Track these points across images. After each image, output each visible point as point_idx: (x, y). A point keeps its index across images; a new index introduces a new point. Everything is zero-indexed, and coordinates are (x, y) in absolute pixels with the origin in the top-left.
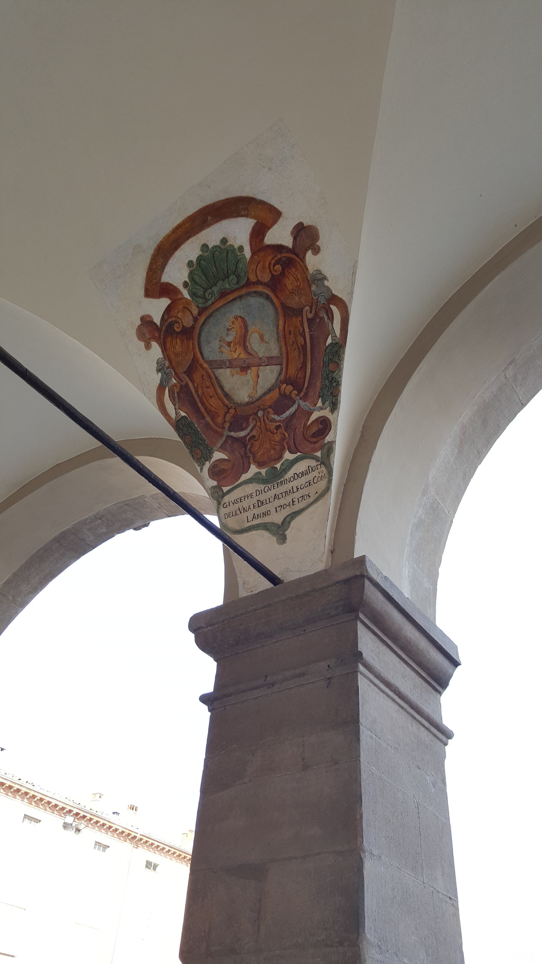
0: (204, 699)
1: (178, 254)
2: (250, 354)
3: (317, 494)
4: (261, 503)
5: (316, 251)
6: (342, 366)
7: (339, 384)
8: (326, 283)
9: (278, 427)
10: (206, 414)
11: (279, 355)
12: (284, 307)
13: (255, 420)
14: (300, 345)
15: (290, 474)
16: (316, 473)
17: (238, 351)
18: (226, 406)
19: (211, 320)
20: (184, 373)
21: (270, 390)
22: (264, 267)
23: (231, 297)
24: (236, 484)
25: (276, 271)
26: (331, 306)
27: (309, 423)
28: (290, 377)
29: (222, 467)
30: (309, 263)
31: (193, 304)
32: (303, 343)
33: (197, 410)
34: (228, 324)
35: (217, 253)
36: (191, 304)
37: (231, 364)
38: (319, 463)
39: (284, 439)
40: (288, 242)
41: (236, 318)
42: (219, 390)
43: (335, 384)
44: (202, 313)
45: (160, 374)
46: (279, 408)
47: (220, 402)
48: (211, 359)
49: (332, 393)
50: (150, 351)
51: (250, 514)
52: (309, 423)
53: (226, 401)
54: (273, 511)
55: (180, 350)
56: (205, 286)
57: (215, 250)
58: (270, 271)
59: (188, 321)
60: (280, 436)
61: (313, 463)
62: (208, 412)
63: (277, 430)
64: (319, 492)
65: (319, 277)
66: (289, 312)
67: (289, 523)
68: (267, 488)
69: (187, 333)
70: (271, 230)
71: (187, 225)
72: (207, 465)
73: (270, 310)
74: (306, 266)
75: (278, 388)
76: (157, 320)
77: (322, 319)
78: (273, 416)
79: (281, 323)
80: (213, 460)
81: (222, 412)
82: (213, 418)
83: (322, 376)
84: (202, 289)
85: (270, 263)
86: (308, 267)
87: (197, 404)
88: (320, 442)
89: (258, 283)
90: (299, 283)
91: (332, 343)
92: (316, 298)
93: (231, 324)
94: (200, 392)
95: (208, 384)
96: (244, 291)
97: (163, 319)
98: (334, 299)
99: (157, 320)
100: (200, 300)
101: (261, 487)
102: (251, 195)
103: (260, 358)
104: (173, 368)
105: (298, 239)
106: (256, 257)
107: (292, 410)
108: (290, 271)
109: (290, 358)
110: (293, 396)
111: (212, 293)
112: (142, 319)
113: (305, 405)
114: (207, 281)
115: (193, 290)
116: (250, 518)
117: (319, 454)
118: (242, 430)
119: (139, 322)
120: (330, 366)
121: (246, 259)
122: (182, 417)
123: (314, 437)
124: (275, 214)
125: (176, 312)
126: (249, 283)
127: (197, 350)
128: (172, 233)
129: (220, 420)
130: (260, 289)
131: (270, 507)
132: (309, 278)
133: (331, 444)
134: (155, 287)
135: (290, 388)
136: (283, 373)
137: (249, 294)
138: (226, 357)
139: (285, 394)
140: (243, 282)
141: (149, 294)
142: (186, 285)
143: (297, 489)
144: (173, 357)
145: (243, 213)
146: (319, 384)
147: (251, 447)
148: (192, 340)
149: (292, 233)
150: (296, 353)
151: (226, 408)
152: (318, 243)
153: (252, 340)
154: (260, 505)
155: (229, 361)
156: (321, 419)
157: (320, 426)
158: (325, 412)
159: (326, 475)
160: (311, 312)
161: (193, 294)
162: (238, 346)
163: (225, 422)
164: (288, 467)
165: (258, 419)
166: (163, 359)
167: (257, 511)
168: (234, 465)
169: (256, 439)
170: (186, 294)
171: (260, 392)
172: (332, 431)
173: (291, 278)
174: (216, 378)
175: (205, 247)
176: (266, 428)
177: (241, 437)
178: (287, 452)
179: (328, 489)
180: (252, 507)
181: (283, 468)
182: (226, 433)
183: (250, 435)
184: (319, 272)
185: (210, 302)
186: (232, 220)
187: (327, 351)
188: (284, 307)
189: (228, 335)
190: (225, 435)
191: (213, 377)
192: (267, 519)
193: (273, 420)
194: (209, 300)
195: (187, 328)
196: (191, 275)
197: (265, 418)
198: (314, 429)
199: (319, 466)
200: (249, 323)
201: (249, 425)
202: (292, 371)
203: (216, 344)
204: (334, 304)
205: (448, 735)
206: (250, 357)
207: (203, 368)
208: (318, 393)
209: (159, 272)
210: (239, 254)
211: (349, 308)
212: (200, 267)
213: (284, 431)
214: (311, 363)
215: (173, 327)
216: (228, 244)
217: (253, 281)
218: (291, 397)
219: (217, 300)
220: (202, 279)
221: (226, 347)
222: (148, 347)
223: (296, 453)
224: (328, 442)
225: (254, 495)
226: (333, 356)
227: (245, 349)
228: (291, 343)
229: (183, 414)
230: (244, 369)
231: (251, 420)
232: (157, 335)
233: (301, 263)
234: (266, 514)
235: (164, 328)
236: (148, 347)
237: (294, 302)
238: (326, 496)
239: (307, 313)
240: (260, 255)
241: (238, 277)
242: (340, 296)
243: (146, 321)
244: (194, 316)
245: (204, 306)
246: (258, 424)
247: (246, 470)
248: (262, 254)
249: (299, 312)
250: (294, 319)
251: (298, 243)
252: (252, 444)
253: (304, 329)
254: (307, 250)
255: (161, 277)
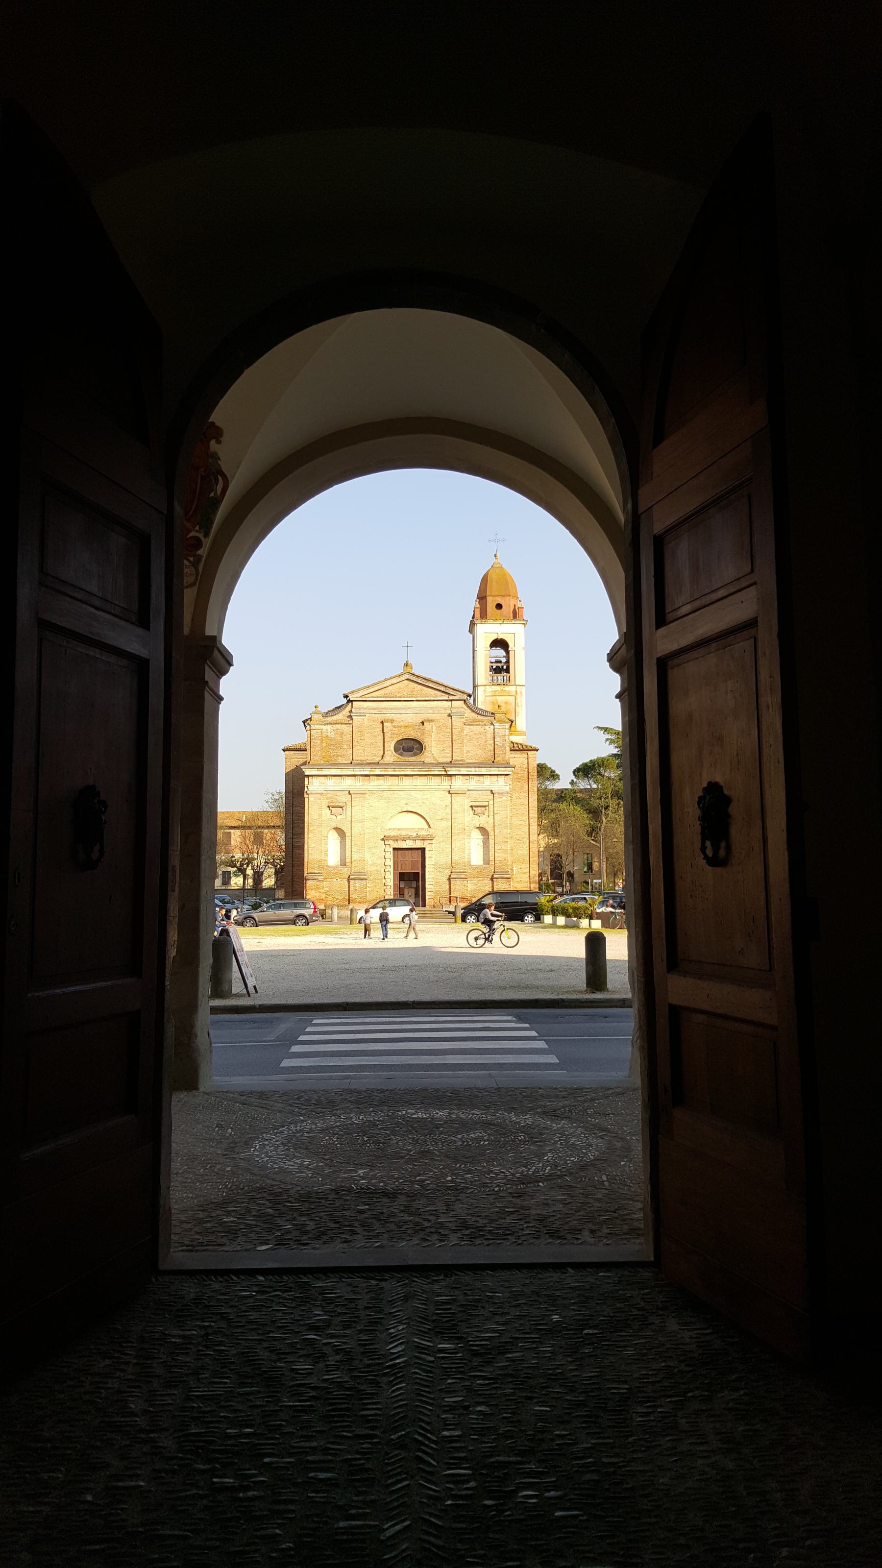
0: (617, 696)
117: (192, 559)
158: (201, 536)
205: (221, 699)
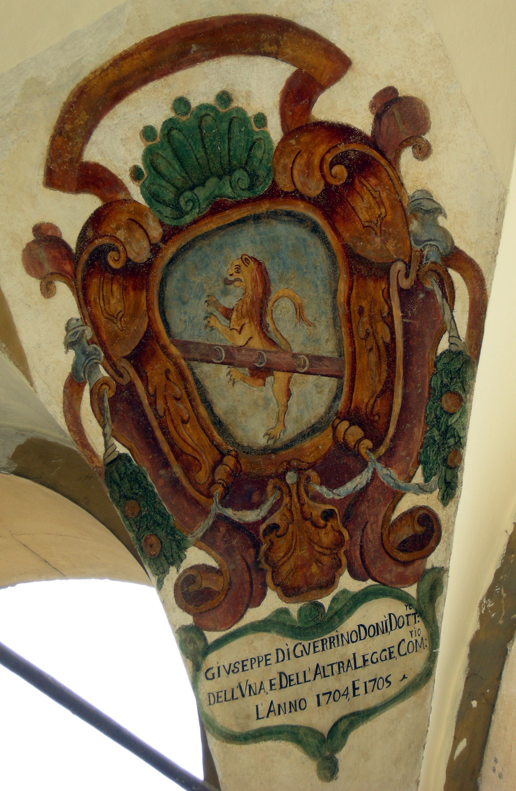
1: (122, 108)
2: (273, 343)
3: (406, 681)
4: (286, 680)
5: (424, 152)
6: (468, 404)
7: (460, 443)
8: (441, 220)
9: (328, 515)
10: (171, 458)
11: (336, 355)
12: (352, 257)
13: (280, 489)
14: (381, 342)
15: (350, 624)
16: (403, 633)
17: (247, 332)
18: (215, 446)
19: (191, 256)
20: (128, 358)
21: (314, 430)
22: (309, 165)
23: (235, 215)
24: (235, 627)
25: (335, 177)
26: (451, 272)
27: (394, 517)
28: (357, 409)
29: (205, 584)
30: (407, 173)
31: (151, 216)
32: (388, 339)
33: (153, 445)
34: (228, 270)
35: (209, 119)
36: (146, 216)
37: (231, 358)
38: (413, 611)
39: (339, 543)
40: (363, 122)
41: (245, 260)
42: (202, 410)
43: (451, 441)
44: (170, 238)
45: (72, 353)
46: (334, 476)
47: (203, 436)
48: (186, 337)
49: (445, 460)
50: (51, 300)
51: (262, 702)
52: (394, 517)
53: (218, 438)
54: (312, 702)
55: (119, 309)
56: (179, 184)
57: (204, 112)
58: (324, 177)
59: (139, 251)
60: (331, 535)
61: (400, 609)
62: (179, 454)
63: (327, 520)
64: (411, 677)
65: (427, 205)
66: (360, 268)
67: (345, 734)
68: (299, 648)
69: (136, 275)
70: (327, 92)
71: (146, 55)
72: (173, 575)
73: (318, 254)
74: (399, 178)
75: (330, 429)
76: (71, 237)
77: (430, 294)
78: (318, 488)
79: (343, 287)
80: (185, 565)
81: (207, 460)
82: (187, 470)
83: (426, 418)
84: (172, 189)
85: (322, 160)
86: (405, 182)
87: (153, 432)
88: (417, 564)
89: (297, 195)
90: (383, 210)
91: (449, 351)
92: (418, 248)
93: (232, 271)
94: (160, 405)
95: (178, 391)
96: (265, 207)
97: (82, 237)
98: (456, 258)
99: (71, 237)
100: (168, 211)
101: (287, 643)
102: (285, 15)
103: (294, 356)
104: (102, 344)
105: (385, 120)
106: (293, 142)
107: (360, 481)
108: (365, 182)
109: (359, 366)
110: (363, 451)
111: (194, 201)
112: (37, 229)
113: (388, 475)
114: (184, 174)
115: (154, 188)
116: (263, 710)
117: (412, 590)
118: (252, 506)
119: (31, 237)
120: (444, 398)
121: (271, 142)
122: (121, 457)
123: (404, 551)
124: (339, 63)
125: (113, 226)
126: (274, 193)
127: (157, 314)
128: (111, 65)
129: (202, 477)
130: (300, 208)
131: (307, 691)
132: (405, 205)
133: (440, 572)
134: (68, 170)
135: (356, 432)
136: (344, 397)
137: (275, 215)
138: (221, 341)
139: (345, 443)
140: (262, 189)
141: (53, 179)
142: (136, 174)
143: (365, 661)
144: (102, 321)
145: (268, 49)
146: (418, 433)
147: (269, 549)
148: (147, 291)
149: (372, 106)
150: (373, 357)
151: (216, 452)
152: (427, 137)
153: (278, 312)
154: (284, 684)
155: (227, 349)
156: (421, 512)
157: (419, 529)
158: (431, 500)
159: (427, 643)
160: (407, 276)
161: (152, 197)
162: (247, 321)
163: (213, 483)
164: (346, 609)
165: (285, 489)
166: (80, 323)
167: (279, 697)
168: (230, 584)
169: (279, 533)
170: (135, 192)
171: (292, 430)
172: (440, 547)
173: (367, 196)
174: (197, 381)
175: (181, 104)
176: (302, 512)
177: (248, 524)
178: (346, 574)
179: (427, 674)
180: (267, 685)
181: (337, 607)
182: (215, 508)
183: (268, 522)
184: (427, 196)
185: (188, 219)
186: (243, 59)
187: (439, 365)
188: (352, 257)
189: (225, 293)
190: (213, 513)
191: (191, 378)
192: (298, 719)
193: (317, 498)
194: (187, 213)
195: (135, 264)
196: (150, 155)
197: (302, 489)
198: (406, 532)
199: (411, 619)
200: (273, 275)
201: (266, 499)
202: (363, 396)
203: (198, 309)
204: (458, 269)
206: (274, 349)
207: (169, 355)
208: (415, 454)
209: (79, 140)
210: (257, 130)
211: (487, 283)
212: (169, 141)
213: (341, 526)
214: (405, 387)
215: (105, 259)
216: (234, 105)
217: (285, 190)
218: (359, 454)
219: (204, 217)
220: (173, 167)
221: (222, 318)
222: (47, 291)
223: (364, 580)
224: (433, 568)
225: (273, 659)
226: (452, 379)
227: (262, 329)
228: (362, 334)
229: (121, 449)
230: (260, 372)
231: (269, 488)
232: (68, 268)
233: (389, 169)
234: (297, 705)
235: (85, 257)
236: (47, 291)
237: (373, 248)
238: (424, 689)
239: (399, 277)
240: (302, 140)
241: (253, 177)
242: (470, 252)
243: (46, 238)
244: (153, 242)
245: (174, 223)
246: (286, 500)
247: (257, 599)
248: (306, 138)
249: (382, 272)
250: (371, 284)
251: (384, 129)
252: (272, 543)
253: (390, 308)
254: (402, 146)
255: (82, 150)
